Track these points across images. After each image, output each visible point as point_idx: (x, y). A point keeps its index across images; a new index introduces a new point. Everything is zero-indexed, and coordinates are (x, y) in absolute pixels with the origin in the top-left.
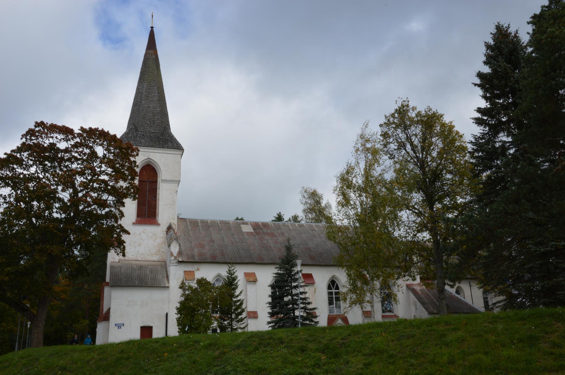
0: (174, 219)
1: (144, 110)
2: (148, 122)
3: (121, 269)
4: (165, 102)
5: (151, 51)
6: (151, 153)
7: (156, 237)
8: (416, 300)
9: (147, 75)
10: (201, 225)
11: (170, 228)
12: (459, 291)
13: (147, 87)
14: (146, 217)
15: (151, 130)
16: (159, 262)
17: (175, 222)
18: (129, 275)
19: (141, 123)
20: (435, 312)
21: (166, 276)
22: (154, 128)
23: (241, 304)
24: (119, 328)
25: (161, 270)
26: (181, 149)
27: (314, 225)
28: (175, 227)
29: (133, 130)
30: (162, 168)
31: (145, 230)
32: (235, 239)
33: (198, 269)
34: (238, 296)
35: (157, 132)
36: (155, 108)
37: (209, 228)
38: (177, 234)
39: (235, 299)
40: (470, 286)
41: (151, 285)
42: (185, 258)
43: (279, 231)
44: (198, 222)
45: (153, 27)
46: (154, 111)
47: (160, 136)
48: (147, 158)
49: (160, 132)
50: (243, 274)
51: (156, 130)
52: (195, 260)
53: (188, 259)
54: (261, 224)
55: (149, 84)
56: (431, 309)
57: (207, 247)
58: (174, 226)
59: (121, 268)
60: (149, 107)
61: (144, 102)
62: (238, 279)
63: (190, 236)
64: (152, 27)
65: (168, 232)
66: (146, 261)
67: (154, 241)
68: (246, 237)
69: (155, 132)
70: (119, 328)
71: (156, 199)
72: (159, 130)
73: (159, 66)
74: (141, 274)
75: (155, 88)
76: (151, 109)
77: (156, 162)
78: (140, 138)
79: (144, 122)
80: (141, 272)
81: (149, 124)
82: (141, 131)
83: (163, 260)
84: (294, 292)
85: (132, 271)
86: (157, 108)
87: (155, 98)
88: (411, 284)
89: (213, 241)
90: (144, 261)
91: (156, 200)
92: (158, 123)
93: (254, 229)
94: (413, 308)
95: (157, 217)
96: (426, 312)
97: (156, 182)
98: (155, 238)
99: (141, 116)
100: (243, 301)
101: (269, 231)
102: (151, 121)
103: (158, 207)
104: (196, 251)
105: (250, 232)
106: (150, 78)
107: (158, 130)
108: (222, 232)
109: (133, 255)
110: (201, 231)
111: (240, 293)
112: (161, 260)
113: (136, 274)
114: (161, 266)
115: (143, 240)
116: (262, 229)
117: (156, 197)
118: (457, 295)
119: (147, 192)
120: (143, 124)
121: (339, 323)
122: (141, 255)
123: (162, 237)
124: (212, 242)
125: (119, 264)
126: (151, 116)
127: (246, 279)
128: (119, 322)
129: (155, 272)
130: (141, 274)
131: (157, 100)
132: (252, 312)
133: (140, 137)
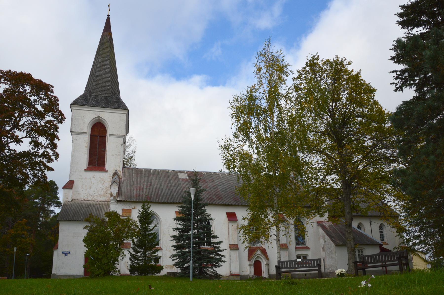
0: (119, 167)
1: (97, 79)
2: (100, 88)
3: (71, 207)
5: (107, 33)
8: (325, 234)
10: (144, 173)
11: (116, 173)
12: (360, 227)
14: (97, 165)
15: (102, 94)
16: (106, 202)
18: (77, 212)
20: (341, 244)
22: (105, 93)
24: (66, 255)
25: (106, 208)
29: (88, 94)
30: (109, 125)
31: (95, 175)
33: (135, 208)
34: (152, 230)
35: (107, 96)
37: (150, 175)
38: (121, 179)
40: (370, 222)
43: (211, 179)
44: (159, 171)
45: (109, 15)
49: (110, 96)
51: (106, 94)
52: (132, 199)
53: (126, 199)
55: (103, 58)
56: (338, 241)
58: (119, 173)
59: (71, 206)
60: (101, 76)
61: (98, 72)
64: (108, 16)
66: (95, 201)
67: (103, 185)
70: (66, 255)
71: (105, 150)
72: (110, 95)
73: (113, 45)
75: (108, 61)
76: (103, 78)
77: (105, 120)
80: (88, 210)
81: (101, 90)
86: (108, 77)
87: (108, 69)
88: (320, 221)
89: (151, 185)
90: (93, 201)
91: (105, 152)
93: (189, 177)
94: (322, 241)
95: (105, 165)
96: (334, 244)
97: (105, 137)
98: (103, 182)
99: (95, 83)
102: (102, 87)
103: (106, 157)
104: (135, 193)
105: (185, 179)
106: (103, 54)
109: (84, 196)
110: (143, 178)
113: (83, 211)
115: (93, 184)
117: (105, 149)
118: (359, 230)
119: (98, 145)
120: (96, 89)
121: (258, 254)
124: (151, 186)
125: (71, 203)
126: (103, 83)
128: (66, 250)
129: (100, 210)
131: (109, 71)
133: (92, 100)
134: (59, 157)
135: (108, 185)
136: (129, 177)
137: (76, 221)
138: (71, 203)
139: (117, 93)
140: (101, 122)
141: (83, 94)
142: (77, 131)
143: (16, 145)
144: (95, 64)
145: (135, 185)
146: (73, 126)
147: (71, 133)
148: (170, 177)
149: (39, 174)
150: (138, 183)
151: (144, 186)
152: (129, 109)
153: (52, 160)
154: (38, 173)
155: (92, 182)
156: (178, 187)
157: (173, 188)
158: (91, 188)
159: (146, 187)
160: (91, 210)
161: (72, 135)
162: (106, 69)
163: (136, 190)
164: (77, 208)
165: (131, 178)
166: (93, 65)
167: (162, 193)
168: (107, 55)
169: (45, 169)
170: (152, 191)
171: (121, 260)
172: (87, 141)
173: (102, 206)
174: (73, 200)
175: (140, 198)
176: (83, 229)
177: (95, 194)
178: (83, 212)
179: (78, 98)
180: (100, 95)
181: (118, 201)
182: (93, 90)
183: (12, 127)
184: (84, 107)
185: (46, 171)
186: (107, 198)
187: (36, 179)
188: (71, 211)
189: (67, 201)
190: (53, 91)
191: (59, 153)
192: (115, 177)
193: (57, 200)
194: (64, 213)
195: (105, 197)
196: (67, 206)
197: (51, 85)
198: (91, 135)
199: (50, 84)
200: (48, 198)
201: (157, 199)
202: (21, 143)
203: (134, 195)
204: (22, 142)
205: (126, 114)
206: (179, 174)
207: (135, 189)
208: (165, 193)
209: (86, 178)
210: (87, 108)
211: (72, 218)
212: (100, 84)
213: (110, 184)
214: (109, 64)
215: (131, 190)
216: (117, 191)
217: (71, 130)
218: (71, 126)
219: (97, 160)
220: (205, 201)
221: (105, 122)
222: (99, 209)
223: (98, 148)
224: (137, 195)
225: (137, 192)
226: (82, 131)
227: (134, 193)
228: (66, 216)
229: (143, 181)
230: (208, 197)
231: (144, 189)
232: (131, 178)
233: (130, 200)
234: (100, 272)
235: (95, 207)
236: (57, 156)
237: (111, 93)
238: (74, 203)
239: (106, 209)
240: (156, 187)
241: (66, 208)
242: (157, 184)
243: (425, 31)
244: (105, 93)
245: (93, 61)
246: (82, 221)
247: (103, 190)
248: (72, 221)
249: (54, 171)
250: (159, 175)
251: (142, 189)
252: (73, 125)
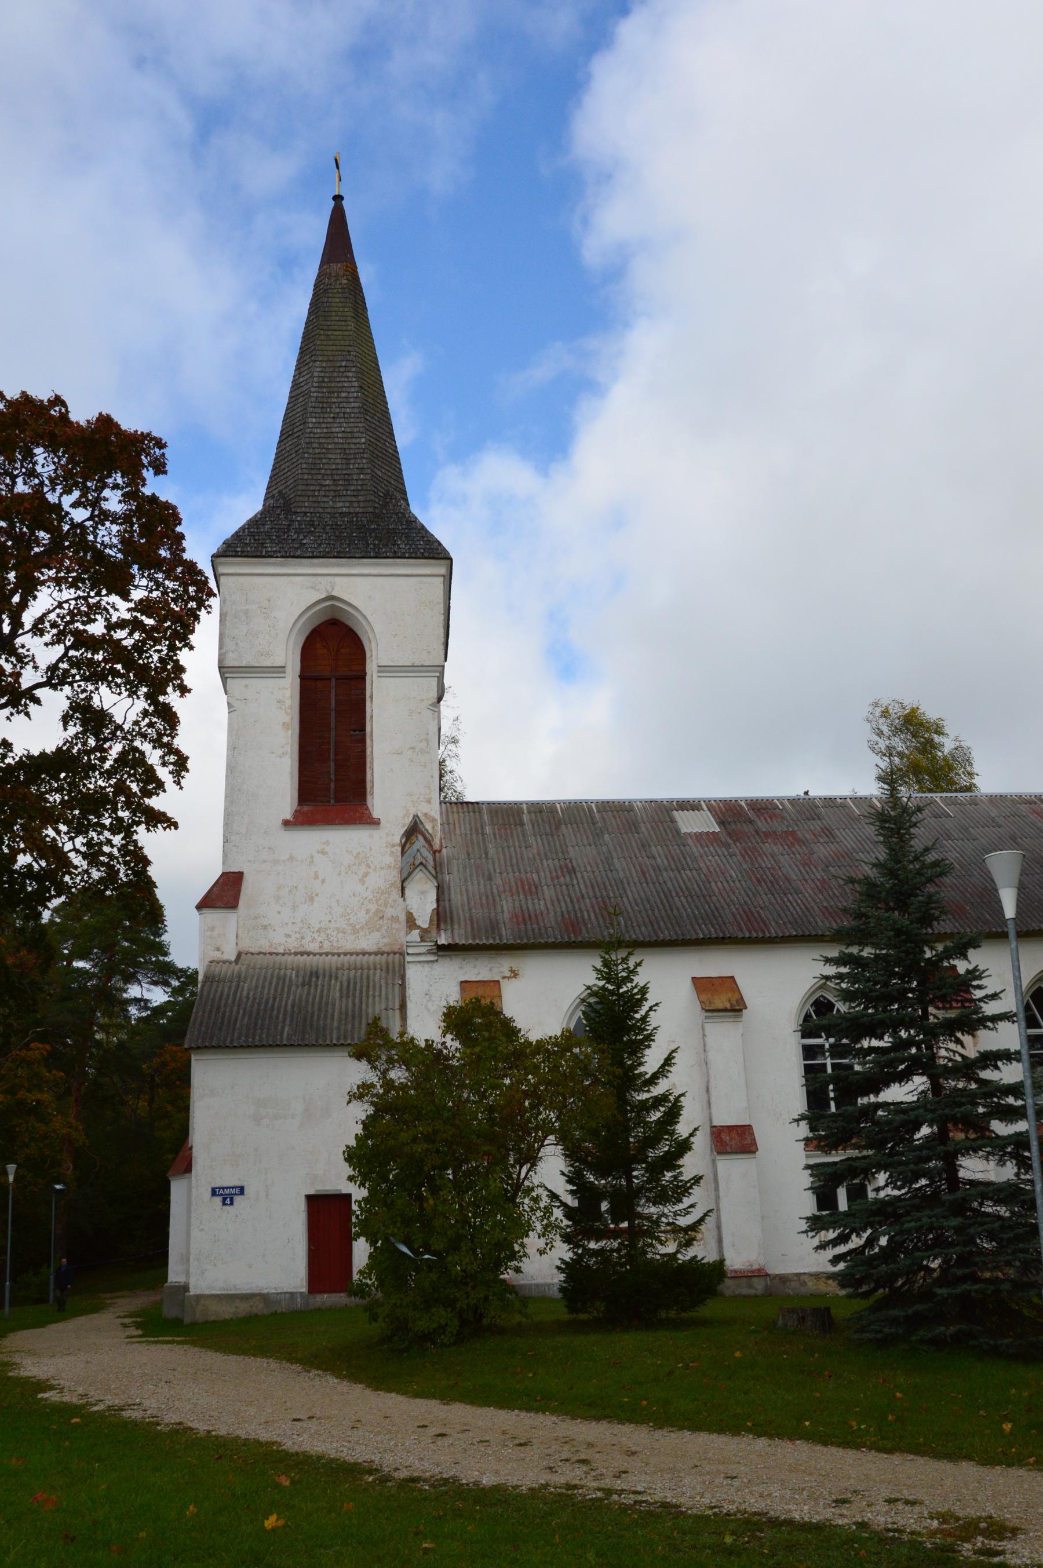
0: (429, 801)
1: (314, 445)
2: (327, 482)
3: (238, 986)
4: (390, 424)
5: (336, 267)
6: (338, 579)
7: (368, 866)
9: (322, 338)
10: (531, 820)
11: (414, 830)
13: (322, 375)
14: (332, 802)
15: (339, 505)
16: (382, 953)
17: (432, 811)
19: (304, 488)
21: (397, 1006)
22: (348, 499)
23: (674, 1113)
24: (228, 1201)
25: (383, 982)
26: (441, 556)
27: (938, 800)
28: (433, 827)
30: (377, 628)
31: (327, 843)
32: (654, 858)
33: (514, 974)
34: (653, 1079)
36: (350, 435)
37: (558, 828)
38: (440, 851)
39: (644, 1096)
41: (338, 1039)
42: (462, 932)
44: (590, 809)
46: (346, 446)
47: (370, 522)
48: (323, 596)
49: (371, 510)
50: (689, 983)
52: (501, 939)
53: (474, 939)
54: (747, 805)
57: (546, 893)
58: (429, 826)
59: (239, 982)
60: (329, 435)
61: (314, 420)
62: (652, 998)
63: (487, 858)
64: (338, 199)
65: (408, 845)
66: (333, 954)
67: (362, 881)
68: (696, 849)
69: (352, 510)
70: (228, 1201)
71: (365, 735)
74: (307, 1001)
75: (350, 374)
76: (336, 440)
78: (299, 534)
79: (313, 482)
80: (308, 993)
82: (305, 513)
83: (396, 948)
84: (946, 1051)
85: (276, 990)
86: (356, 435)
87: (353, 405)
89: (572, 871)
90: (327, 954)
91: (363, 741)
92: (360, 483)
93: (721, 823)
95: (369, 798)
97: (360, 678)
98: (363, 869)
99: (304, 466)
100: (677, 1099)
101: (778, 826)
102: (335, 477)
104: (507, 907)
107: (361, 505)
108: (606, 836)
109: (289, 936)
110: (531, 839)
111: (663, 1066)
112: (386, 949)
113: (290, 1002)
114: (387, 968)
115: (323, 881)
116: (751, 822)
117: (363, 729)
119: (333, 714)
120: (312, 488)
122: (316, 935)
123: (389, 867)
124: (569, 872)
125: (237, 968)
126: (338, 461)
127: (701, 1002)
128: (228, 1180)
129: (361, 993)
130: (307, 1001)
131: (356, 410)
132: (731, 1128)
133: (298, 531)
134: (188, 771)
135: (386, 881)
136: (472, 843)
137: (263, 1046)
138: (237, 968)
139: (398, 496)
140: (339, 618)
141: (262, 513)
142: (244, 664)
143: (8, 718)
144: (301, 390)
145: (501, 873)
146: (229, 644)
147: (222, 674)
148: (643, 829)
149: (112, 846)
150: (512, 865)
151: (542, 874)
152: (452, 555)
153: (160, 785)
154: (109, 842)
155: (316, 872)
156: (688, 872)
157: (665, 874)
158: (316, 899)
159: (552, 879)
160: (321, 997)
161: (224, 680)
162: (345, 405)
163: (512, 895)
164: (263, 987)
165: (478, 843)
166: (290, 397)
167: (625, 899)
168: (347, 348)
169: (138, 824)
170: (579, 894)
171: (542, 1252)
172: (288, 703)
173: (365, 972)
174: (243, 957)
175: (533, 930)
176: (349, 1102)
177: (333, 925)
178: (289, 1008)
179: (242, 529)
180: (329, 510)
181: (441, 948)
182: (299, 493)
184: (268, 564)
185: (142, 835)
186: (383, 937)
187: (99, 870)
188: (239, 1005)
189: (218, 962)
190: (164, 465)
191: (185, 750)
192: (415, 847)
193: (161, 958)
194: (209, 1017)
195: (377, 935)
196: (218, 982)
197: (155, 438)
198: (302, 677)
199: (149, 434)
200: (126, 952)
201: (607, 928)
202: (32, 708)
203: (506, 915)
204: (37, 701)
205: (442, 579)
206: (678, 815)
207: (504, 892)
208: (635, 900)
209: (291, 858)
210: (282, 565)
211: (247, 1037)
212: (326, 467)
213: (394, 876)
214: (356, 384)
215: (487, 897)
216: (435, 906)
217: (220, 661)
218: (221, 648)
219: (333, 777)
220: (820, 923)
221: (360, 618)
222: (355, 989)
223: (333, 725)
224: (516, 916)
225: (517, 904)
226: (268, 663)
227: (505, 909)
228: (220, 1029)
229: (531, 855)
230: (825, 907)
231: (545, 888)
232: (478, 843)
233: (494, 939)
234: (443, 1322)
235: (337, 978)
236: (181, 764)
237: (372, 498)
238: (247, 970)
239: (387, 984)
240: (591, 874)
241: (218, 994)
242: (592, 863)
244: (348, 499)
245: (292, 379)
246: (292, 1045)
247: (366, 902)
248: (249, 1046)
249: (176, 828)
250: (594, 824)
251: (533, 889)
252: (227, 640)
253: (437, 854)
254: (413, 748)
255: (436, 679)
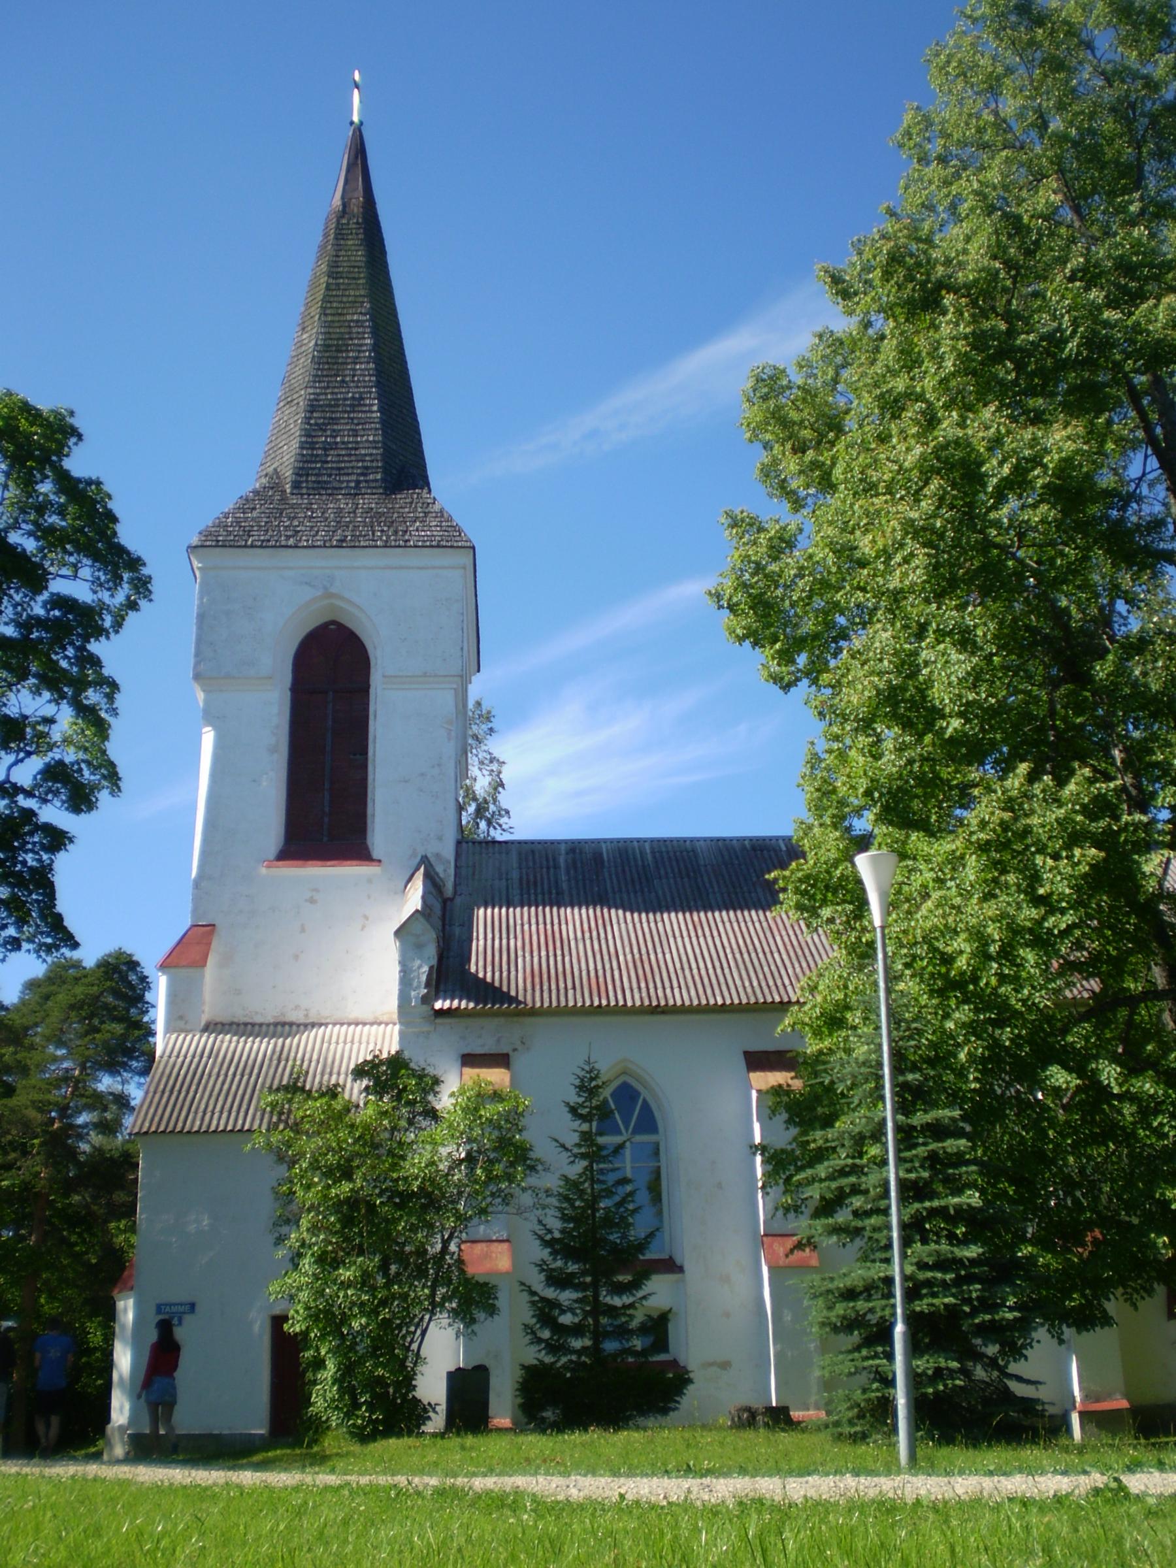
14: (325, 839)
38: (452, 900)
91: (365, 766)
152: (472, 532)
183: (48, 619)
219: (327, 809)
241: (300, 1055)
243: (15, 635)
253: (449, 903)
254: (422, 775)
255: (453, 692)
